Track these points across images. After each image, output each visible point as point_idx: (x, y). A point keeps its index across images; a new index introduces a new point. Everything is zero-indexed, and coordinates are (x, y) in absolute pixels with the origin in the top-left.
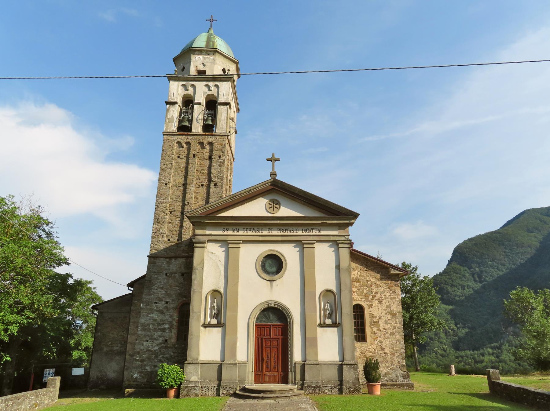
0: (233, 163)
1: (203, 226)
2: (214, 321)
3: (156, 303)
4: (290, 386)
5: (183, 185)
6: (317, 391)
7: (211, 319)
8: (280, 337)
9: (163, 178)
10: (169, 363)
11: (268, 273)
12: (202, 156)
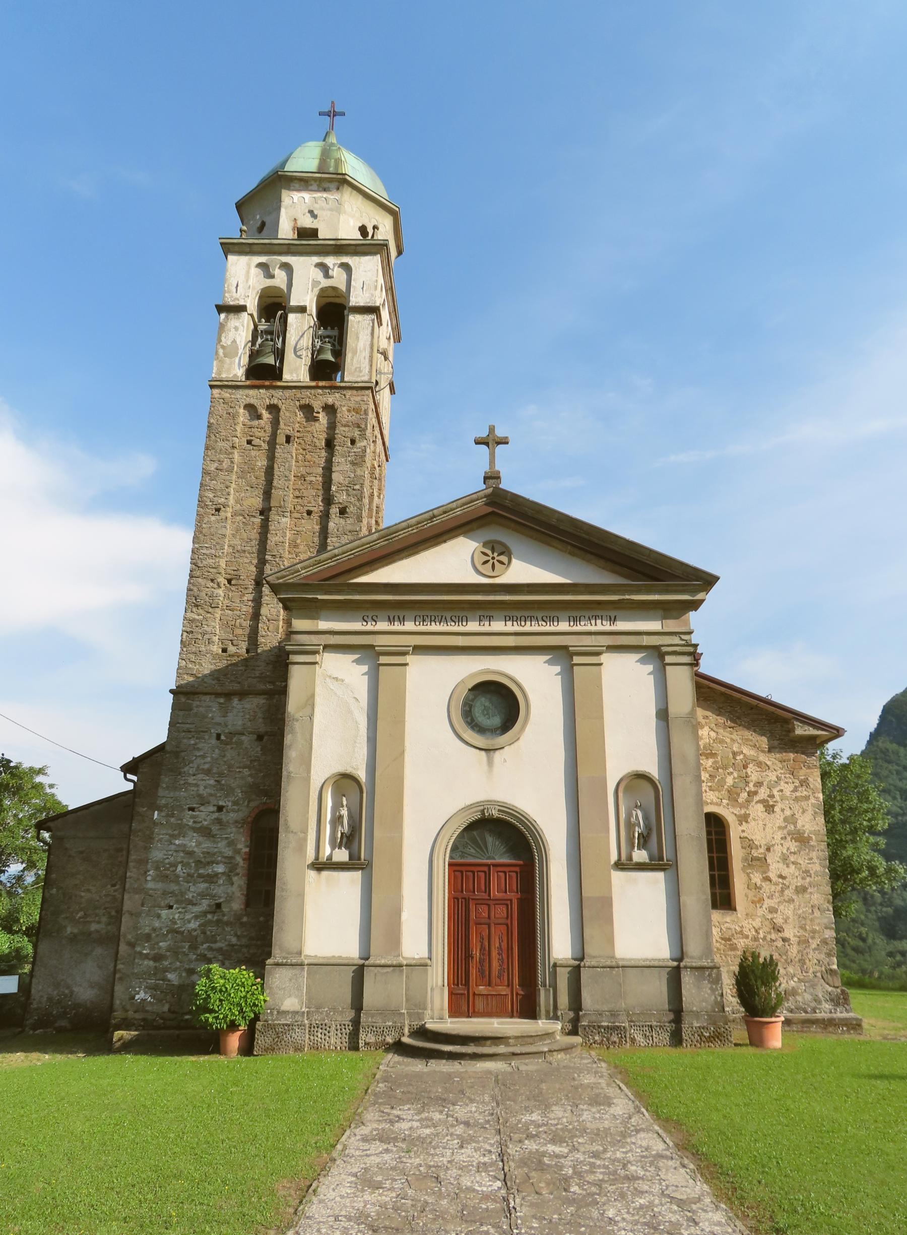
0: (385, 465)
1: (313, 609)
2: (342, 855)
3: (192, 809)
4: (542, 1025)
5: (262, 513)
6: (615, 1038)
7: (333, 848)
8: (514, 896)
9: (211, 495)
10: (227, 963)
11: (480, 729)
12: (308, 439)
